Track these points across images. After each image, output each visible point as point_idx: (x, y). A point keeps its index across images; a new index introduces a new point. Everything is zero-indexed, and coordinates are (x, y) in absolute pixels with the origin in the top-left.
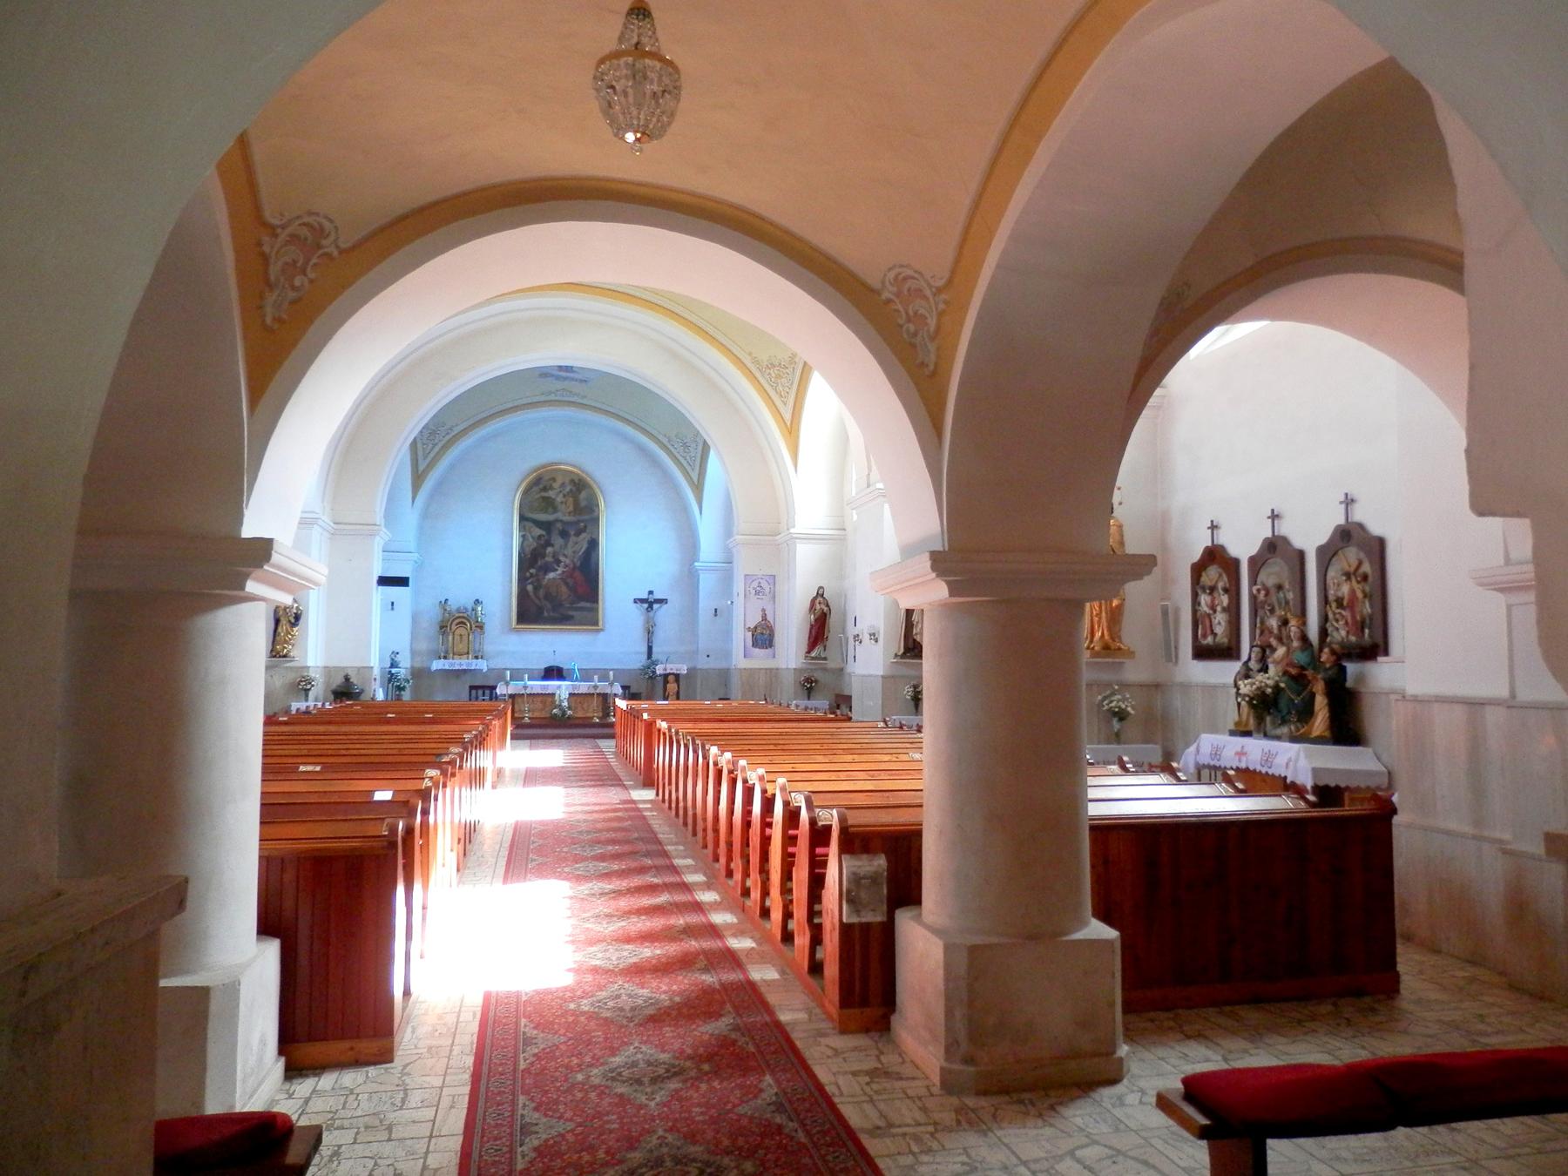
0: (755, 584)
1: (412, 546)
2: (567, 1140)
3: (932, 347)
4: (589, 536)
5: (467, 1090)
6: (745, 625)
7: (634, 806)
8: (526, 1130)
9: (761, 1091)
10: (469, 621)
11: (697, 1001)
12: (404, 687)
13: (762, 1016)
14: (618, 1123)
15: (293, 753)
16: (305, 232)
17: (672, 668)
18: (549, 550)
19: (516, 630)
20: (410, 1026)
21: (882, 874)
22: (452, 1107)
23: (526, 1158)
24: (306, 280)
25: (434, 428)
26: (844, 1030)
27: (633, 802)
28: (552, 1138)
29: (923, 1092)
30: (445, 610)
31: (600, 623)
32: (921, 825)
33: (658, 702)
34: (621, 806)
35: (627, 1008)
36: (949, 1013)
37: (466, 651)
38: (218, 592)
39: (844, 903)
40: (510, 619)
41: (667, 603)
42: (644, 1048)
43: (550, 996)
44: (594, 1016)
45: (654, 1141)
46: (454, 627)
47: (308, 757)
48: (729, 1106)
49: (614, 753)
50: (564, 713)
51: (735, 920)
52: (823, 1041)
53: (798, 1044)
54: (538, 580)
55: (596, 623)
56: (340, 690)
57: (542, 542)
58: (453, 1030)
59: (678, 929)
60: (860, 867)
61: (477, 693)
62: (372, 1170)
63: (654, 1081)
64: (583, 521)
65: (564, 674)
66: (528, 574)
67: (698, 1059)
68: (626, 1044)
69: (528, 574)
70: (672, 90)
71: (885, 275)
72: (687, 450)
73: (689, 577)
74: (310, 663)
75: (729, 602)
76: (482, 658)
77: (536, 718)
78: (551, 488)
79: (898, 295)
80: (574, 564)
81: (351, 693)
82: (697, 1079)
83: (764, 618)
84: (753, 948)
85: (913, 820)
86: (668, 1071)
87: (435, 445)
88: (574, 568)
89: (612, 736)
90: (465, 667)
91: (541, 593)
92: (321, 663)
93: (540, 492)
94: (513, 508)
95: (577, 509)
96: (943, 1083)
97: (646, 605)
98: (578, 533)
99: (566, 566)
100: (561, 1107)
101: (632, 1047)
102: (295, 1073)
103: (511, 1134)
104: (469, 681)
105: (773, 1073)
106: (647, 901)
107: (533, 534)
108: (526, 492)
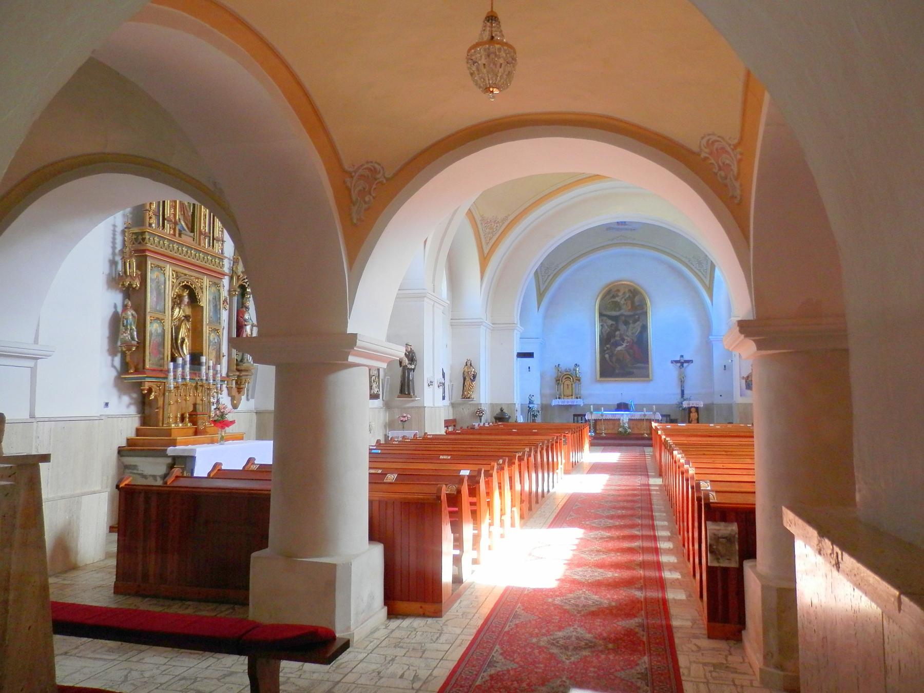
2: (510, 674)
3: (737, 185)
4: (641, 324)
5: (472, 637)
7: (647, 487)
8: (491, 664)
9: (637, 665)
10: (572, 377)
11: (624, 607)
12: (537, 415)
15: (447, 449)
16: (367, 173)
17: (693, 403)
18: (617, 333)
19: (597, 381)
20: (459, 600)
21: (734, 537)
23: (483, 679)
24: (371, 198)
26: (711, 636)
27: (649, 485)
28: (503, 671)
29: (746, 683)
31: (651, 375)
32: (755, 505)
33: (679, 425)
34: (640, 488)
35: (581, 605)
37: (571, 394)
38: (339, 362)
40: (596, 375)
41: (692, 362)
42: (579, 629)
43: (540, 593)
44: (559, 607)
45: (558, 682)
47: (444, 452)
48: (612, 671)
50: (626, 431)
51: (676, 561)
52: (694, 641)
53: (677, 641)
55: (648, 376)
56: (499, 416)
57: (613, 328)
60: (718, 530)
61: (577, 419)
62: (405, 671)
63: (575, 649)
64: (637, 315)
66: (605, 348)
67: (607, 640)
68: (570, 625)
69: (605, 348)
70: (512, 61)
71: (700, 142)
72: (700, 266)
73: (707, 346)
74: (482, 401)
75: (730, 361)
77: (609, 434)
78: (617, 296)
79: (711, 153)
81: (504, 418)
82: (601, 652)
84: (678, 579)
85: (750, 502)
86: (586, 644)
89: (651, 446)
90: (570, 404)
91: (614, 359)
92: (488, 401)
93: (611, 298)
94: (595, 309)
95: (634, 307)
98: (635, 321)
99: (628, 342)
102: (394, 616)
103: (508, 618)
104: (573, 411)
105: (650, 655)
106: (626, 544)
107: (608, 324)
108: (603, 299)
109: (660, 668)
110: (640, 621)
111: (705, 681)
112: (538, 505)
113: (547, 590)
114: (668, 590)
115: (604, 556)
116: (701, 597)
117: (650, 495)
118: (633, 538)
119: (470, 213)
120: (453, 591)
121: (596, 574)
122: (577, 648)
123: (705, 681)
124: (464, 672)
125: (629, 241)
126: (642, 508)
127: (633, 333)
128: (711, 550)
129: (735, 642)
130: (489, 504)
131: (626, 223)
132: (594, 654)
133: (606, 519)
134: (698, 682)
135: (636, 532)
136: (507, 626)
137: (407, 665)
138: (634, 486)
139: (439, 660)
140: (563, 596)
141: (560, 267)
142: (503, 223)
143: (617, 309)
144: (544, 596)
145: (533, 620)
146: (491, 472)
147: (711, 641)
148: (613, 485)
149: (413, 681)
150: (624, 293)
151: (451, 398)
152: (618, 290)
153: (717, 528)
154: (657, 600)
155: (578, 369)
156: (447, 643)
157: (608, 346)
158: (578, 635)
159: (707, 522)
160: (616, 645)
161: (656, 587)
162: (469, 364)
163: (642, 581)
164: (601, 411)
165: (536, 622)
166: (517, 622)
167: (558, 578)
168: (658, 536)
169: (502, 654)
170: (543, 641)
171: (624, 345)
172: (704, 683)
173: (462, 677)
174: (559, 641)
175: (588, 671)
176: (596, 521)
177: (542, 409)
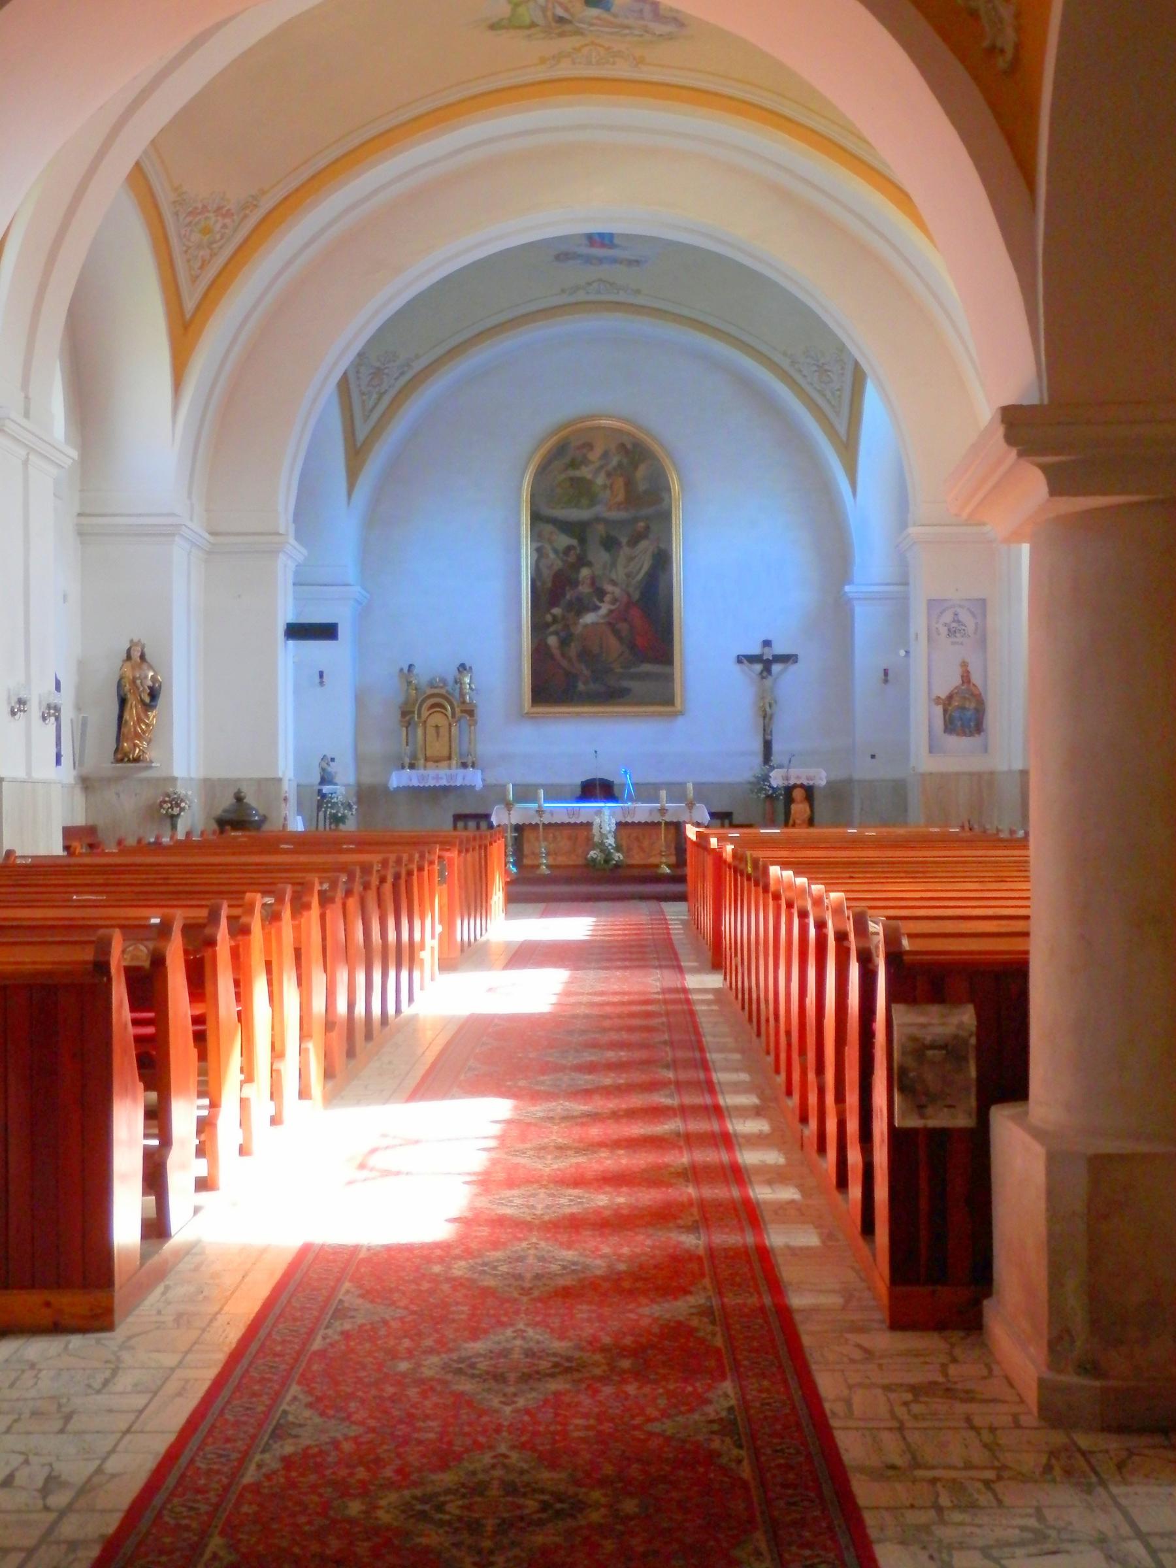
0: (948, 617)
1: (352, 575)
6: (929, 693)
7: (682, 996)
9: (708, 1402)
13: (760, 1296)
14: (436, 1433)
17: (799, 775)
18: (585, 572)
19: (529, 716)
22: (179, 1394)
25: (378, 364)
26: (899, 1322)
27: (685, 991)
30: (409, 683)
31: (678, 701)
35: (529, 1276)
36: (1055, 1281)
37: (445, 753)
39: (896, 1090)
42: (530, 1332)
45: (487, 1458)
46: (425, 713)
48: (638, 1421)
49: (683, 922)
51: (781, 1160)
53: (806, 1340)
54: (567, 626)
55: (669, 701)
56: (229, 816)
58: (228, 1293)
59: (672, 1170)
60: (923, 1026)
65: (616, 791)
66: (549, 618)
69: (549, 618)
74: (179, 771)
75: (902, 653)
76: (473, 766)
78: (585, 461)
80: (629, 595)
83: (966, 678)
87: (381, 395)
88: (630, 604)
89: (682, 897)
91: (573, 650)
93: (566, 469)
95: (633, 498)
96: (1042, 1407)
97: (758, 667)
98: (635, 541)
99: (615, 601)
100: (353, 1405)
101: (511, 1329)
103: (253, 1438)
104: (453, 806)
105: (739, 1377)
106: (638, 1129)
108: (543, 470)
109: (768, 1404)
110: (702, 1301)
111: (895, 1424)
112: (370, 1045)
113: (423, 1246)
114: (769, 1226)
115: (581, 1159)
116: (868, 1228)
117: (692, 1013)
118: (657, 1113)
119: (138, 177)
120: (144, 1256)
121: (563, 1201)
122: (529, 1377)
123: (895, 1424)
124: (171, 1511)
125: (622, 297)
126: (671, 1044)
127: (628, 575)
128: (899, 1081)
129: (961, 1334)
130: (244, 1018)
131: (616, 241)
132: (584, 1386)
133: (573, 1074)
134: (878, 1429)
135: (662, 1099)
136: (252, 1467)
137: (21, 1453)
138: (644, 993)
139: (119, 1435)
140: (475, 1257)
141: (418, 366)
142: (246, 216)
143: (584, 501)
144: (418, 1261)
145: (394, 1319)
146: (244, 920)
147: (899, 1335)
148: (583, 994)
149: (45, 1491)
150: (605, 455)
151: (78, 762)
152: (589, 446)
153: (922, 1020)
154: (738, 1255)
155: (467, 680)
156: (139, 1392)
157: (557, 611)
158: (532, 1344)
159: (894, 1007)
160: (641, 1361)
161: (735, 1222)
162: (136, 655)
163: (695, 1210)
164: (535, 799)
165: (403, 1323)
166: (347, 1326)
167: (455, 1214)
168: (727, 1108)
169: (310, 1405)
170: (431, 1366)
171: (605, 608)
172: (890, 1429)
173: (199, 1468)
174: (475, 1363)
175: (571, 1427)
176: (546, 1078)
177: (360, 801)
